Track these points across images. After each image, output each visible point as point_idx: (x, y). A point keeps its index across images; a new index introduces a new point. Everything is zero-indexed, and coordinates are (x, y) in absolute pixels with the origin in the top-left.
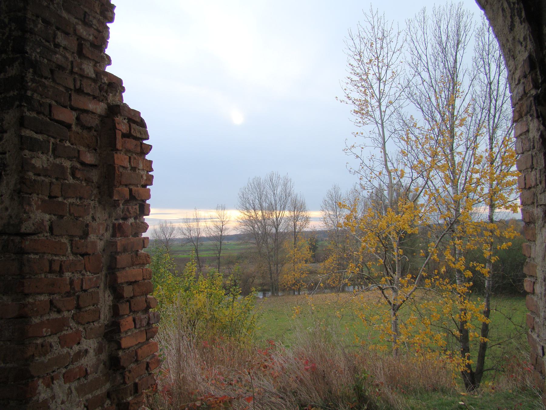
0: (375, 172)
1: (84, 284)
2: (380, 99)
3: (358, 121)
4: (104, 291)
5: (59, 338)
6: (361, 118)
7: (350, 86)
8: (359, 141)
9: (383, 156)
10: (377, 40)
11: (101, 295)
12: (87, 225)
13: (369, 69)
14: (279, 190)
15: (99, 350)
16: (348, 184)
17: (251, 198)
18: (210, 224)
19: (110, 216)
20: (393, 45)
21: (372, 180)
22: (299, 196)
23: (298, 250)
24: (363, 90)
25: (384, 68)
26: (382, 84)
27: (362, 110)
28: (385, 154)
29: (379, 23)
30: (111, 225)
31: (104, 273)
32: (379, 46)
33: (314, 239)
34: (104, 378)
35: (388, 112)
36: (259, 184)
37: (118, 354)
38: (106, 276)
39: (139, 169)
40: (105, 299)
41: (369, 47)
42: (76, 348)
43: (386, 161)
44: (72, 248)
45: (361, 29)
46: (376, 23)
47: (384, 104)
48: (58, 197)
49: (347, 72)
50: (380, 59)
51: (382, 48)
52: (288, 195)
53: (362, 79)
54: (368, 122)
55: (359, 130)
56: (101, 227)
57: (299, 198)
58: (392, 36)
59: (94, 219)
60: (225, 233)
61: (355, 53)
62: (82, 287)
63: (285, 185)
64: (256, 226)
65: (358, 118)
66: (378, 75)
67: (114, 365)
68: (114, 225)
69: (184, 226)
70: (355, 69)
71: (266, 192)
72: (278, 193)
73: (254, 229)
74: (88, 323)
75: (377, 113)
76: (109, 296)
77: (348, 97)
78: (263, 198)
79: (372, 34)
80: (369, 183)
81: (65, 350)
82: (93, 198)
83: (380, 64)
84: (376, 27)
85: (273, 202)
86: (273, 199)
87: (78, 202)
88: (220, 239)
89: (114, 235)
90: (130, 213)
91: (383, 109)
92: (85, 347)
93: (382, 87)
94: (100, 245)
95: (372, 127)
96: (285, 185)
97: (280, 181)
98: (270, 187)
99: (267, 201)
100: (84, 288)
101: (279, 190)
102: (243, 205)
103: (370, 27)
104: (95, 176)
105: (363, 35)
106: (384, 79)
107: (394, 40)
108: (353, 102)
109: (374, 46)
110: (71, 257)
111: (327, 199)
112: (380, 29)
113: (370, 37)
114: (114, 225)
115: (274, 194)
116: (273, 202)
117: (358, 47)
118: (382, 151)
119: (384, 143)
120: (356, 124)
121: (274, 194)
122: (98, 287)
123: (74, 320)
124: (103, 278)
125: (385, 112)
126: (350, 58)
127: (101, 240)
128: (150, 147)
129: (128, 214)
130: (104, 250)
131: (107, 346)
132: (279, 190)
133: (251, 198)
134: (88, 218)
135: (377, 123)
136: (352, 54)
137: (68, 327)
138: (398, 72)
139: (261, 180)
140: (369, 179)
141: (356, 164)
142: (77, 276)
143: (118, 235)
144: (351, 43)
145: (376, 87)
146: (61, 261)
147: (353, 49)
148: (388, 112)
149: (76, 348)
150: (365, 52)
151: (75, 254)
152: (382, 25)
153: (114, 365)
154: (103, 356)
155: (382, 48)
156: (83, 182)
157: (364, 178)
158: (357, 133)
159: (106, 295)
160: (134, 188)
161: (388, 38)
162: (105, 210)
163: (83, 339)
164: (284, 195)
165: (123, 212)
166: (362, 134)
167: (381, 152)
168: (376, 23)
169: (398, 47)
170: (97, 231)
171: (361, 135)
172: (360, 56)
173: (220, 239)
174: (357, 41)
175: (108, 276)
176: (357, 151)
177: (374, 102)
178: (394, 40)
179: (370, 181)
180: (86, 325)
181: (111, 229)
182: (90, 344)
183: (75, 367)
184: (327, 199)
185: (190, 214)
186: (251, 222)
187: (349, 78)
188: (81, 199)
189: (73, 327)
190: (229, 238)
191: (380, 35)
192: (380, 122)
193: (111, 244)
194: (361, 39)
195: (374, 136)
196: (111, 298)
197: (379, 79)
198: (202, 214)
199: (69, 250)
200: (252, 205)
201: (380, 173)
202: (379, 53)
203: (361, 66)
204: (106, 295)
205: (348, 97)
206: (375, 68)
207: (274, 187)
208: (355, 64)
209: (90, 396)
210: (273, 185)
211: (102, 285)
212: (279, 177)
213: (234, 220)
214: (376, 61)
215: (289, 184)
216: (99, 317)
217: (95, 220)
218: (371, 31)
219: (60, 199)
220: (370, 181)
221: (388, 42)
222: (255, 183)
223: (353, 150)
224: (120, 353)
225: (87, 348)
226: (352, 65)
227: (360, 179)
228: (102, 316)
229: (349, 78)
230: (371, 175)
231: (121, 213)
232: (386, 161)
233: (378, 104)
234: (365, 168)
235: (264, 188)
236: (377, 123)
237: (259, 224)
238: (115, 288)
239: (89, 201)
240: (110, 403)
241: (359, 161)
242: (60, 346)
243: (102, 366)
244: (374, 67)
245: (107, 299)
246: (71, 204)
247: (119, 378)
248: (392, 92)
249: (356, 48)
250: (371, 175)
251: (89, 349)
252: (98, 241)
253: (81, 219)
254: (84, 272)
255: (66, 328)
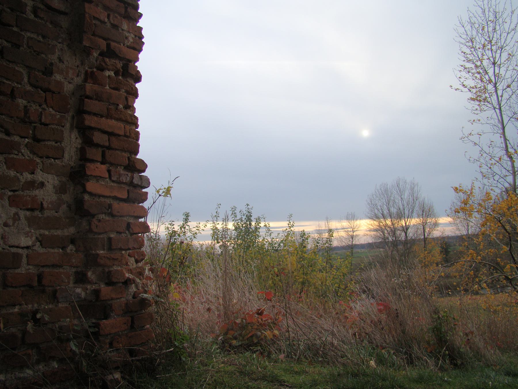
0: (495, 158)
1: (43, 117)
2: (496, 84)
3: (474, 109)
4: (70, 132)
5: (5, 158)
6: (479, 105)
7: (464, 74)
8: (477, 128)
9: (503, 142)
10: (489, 23)
11: (66, 134)
12: (52, 64)
13: (483, 55)
14: (406, 195)
15: (61, 190)
16: (469, 177)
17: (379, 204)
18: (343, 234)
19: (82, 64)
20: (506, 26)
21: (492, 167)
22: (426, 199)
23: (428, 253)
24: (478, 76)
25: (499, 52)
26: (496, 68)
27: (479, 98)
28: (505, 140)
29: (489, 6)
30: (83, 72)
31: (71, 114)
32: (490, 29)
33: (447, 247)
34: (67, 220)
35: (506, 96)
36: (386, 191)
37: (84, 198)
38: (73, 117)
39: (123, 30)
40: (71, 142)
41: (481, 32)
42: (27, 176)
43: (506, 146)
44: (29, 78)
45: (471, 15)
46: (486, 6)
47: (500, 87)
48: (13, 27)
49: (458, 60)
50: (493, 42)
51: (494, 29)
52: (415, 199)
53: (476, 66)
54: (486, 108)
55: (475, 117)
56: (71, 72)
57: (426, 201)
58: (504, 16)
59: (60, 60)
60: (356, 242)
61: (467, 40)
62: (40, 120)
63: (412, 189)
64: (386, 232)
65: (474, 105)
66: (492, 59)
67: (80, 210)
68: (86, 72)
69: (316, 236)
70: (468, 56)
71: (394, 197)
72: (405, 197)
73: (384, 235)
74: (48, 157)
75: (494, 97)
76: (77, 138)
77: (463, 85)
78: (391, 203)
79: (483, 18)
80: (489, 170)
81: (12, 173)
82: (60, 40)
83: (494, 48)
84: (487, 10)
85: (401, 207)
86: (400, 204)
87: (40, 38)
88: (351, 248)
89: (85, 80)
90: (106, 65)
91: (500, 93)
92: (41, 179)
93: (497, 71)
94: (68, 88)
95: (490, 113)
96: (412, 189)
97: (407, 186)
98: (397, 192)
99: (395, 206)
100: (43, 121)
101: (406, 195)
102: (372, 211)
103: (480, 11)
104: (64, 22)
105: (474, 20)
106: (499, 63)
107: (508, 20)
108: (469, 90)
109: (486, 29)
110: (29, 88)
111: (455, 201)
112: (491, 10)
113: (481, 21)
114: (86, 72)
115: (402, 198)
116: (401, 207)
117: (469, 33)
118: (502, 136)
119: (503, 128)
120: (473, 112)
121: (402, 198)
122: (63, 127)
123: (27, 148)
124: (69, 119)
125: (502, 96)
126: (462, 46)
127: (70, 83)
128: (141, 15)
129: (103, 64)
130: (73, 94)
131: (72, 188)
132: (406, 195)
133: (379, 204)
134: (54, 58)
135: (494, 108)
136: (463, 41)
137: (19, 152)
138: (514, 53)
139: (388, 186)
140: (489, 166)
141: (475, 152)
142: (34, 107)
143: (89, 81)
144: (462, 30)
145: (491, 72)
146: (13, 87)
147: (464, 36)
148: (506, 96)
149: (27, 176)
150: (477, 38)
151: (31, 85)
152: (494, 7)
153: (80, 210)
154: (67, 197)
155: (494, 29)
156: (48, 23)
157: (483, 165)
158: (474, 121)
159: (73, 136)
160: (113, 44)
161: (501, 20)
162: (76, 55)
163: (39, 170)
164: (411, 200)
165: (96, 61)
166: (479, 120)
167: (501, 137)
168: (486, 6)
169: (513, 26)
170: (64, 73)
171: (478, 122)
172: (472, 42)
173: (351, 248)
174: (468, 27)
175: (75, 118)
176: (475, 138)
177: (490, 87)
178: (508, 20)
179: (490, 168)
180: (45, 159)
181: (83, 76)
182: (51, 181)
183: (25, 194)
184: (455, 201)
185: (323, 225)
186: (380, 229)
187: (462, 66)
188: (44, 37)
189: (25, 154)
190: (362, 246)
191: (492, 18)
192: (497, 107)
193: (81, 87)
194: (472, 24)
195: (492, 121)
196: (79, 141)
197: (494, 64)
198: (334, 224)
199: (26, 80)
200: (380, 211)
201: (500, 159)
202: (491, 36)
203: (474, 53)
204: (73, 136)
205: (463, 85)
206: (489, 53)
207: (401, 193)
208: (468, 51)
209: (47, 233)
210: (400, 191)
211: (68, 125)
212: (405, 182)
213: (364, 229)
214: (490, 45)
215: (416, 188)
216: (63, 156)
217: (63, 62)
218: (481, 15)
219: (15, 29)
220: (490, 168)
221: (501, 22)
222: (382, 189)
223: (471, 137)
224: (86, 197)
225: (43, 180)
226: (465, 53)
227: (480, 167)
228: (66, 156)
229: (462, 66)
230: (491, 162)
231: (95, 62)
232: (506, 146)
233: (494, 89)
234: (485, 155)
235: (392, 193)
236: (494, 108)
237: (388, 229)
238: (85, 132)
239: (55, 42)
240: (74, 249)
241: (478, 148)
242: (5, 167)
243: (64, 207)
244: (487, 52)
245: (74, 140)
246: (30, 38)
247: (84, 224)
248: (509, 74)
249: (467, 35)
250: (491, 162)
251: (46, 183)
252: (66, 83)
253: (43, 56)
254: (44, 106)
255: (16, 152)
